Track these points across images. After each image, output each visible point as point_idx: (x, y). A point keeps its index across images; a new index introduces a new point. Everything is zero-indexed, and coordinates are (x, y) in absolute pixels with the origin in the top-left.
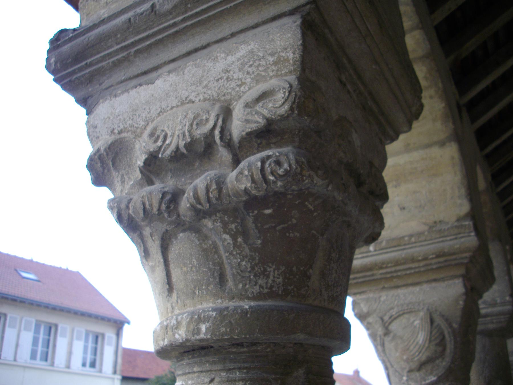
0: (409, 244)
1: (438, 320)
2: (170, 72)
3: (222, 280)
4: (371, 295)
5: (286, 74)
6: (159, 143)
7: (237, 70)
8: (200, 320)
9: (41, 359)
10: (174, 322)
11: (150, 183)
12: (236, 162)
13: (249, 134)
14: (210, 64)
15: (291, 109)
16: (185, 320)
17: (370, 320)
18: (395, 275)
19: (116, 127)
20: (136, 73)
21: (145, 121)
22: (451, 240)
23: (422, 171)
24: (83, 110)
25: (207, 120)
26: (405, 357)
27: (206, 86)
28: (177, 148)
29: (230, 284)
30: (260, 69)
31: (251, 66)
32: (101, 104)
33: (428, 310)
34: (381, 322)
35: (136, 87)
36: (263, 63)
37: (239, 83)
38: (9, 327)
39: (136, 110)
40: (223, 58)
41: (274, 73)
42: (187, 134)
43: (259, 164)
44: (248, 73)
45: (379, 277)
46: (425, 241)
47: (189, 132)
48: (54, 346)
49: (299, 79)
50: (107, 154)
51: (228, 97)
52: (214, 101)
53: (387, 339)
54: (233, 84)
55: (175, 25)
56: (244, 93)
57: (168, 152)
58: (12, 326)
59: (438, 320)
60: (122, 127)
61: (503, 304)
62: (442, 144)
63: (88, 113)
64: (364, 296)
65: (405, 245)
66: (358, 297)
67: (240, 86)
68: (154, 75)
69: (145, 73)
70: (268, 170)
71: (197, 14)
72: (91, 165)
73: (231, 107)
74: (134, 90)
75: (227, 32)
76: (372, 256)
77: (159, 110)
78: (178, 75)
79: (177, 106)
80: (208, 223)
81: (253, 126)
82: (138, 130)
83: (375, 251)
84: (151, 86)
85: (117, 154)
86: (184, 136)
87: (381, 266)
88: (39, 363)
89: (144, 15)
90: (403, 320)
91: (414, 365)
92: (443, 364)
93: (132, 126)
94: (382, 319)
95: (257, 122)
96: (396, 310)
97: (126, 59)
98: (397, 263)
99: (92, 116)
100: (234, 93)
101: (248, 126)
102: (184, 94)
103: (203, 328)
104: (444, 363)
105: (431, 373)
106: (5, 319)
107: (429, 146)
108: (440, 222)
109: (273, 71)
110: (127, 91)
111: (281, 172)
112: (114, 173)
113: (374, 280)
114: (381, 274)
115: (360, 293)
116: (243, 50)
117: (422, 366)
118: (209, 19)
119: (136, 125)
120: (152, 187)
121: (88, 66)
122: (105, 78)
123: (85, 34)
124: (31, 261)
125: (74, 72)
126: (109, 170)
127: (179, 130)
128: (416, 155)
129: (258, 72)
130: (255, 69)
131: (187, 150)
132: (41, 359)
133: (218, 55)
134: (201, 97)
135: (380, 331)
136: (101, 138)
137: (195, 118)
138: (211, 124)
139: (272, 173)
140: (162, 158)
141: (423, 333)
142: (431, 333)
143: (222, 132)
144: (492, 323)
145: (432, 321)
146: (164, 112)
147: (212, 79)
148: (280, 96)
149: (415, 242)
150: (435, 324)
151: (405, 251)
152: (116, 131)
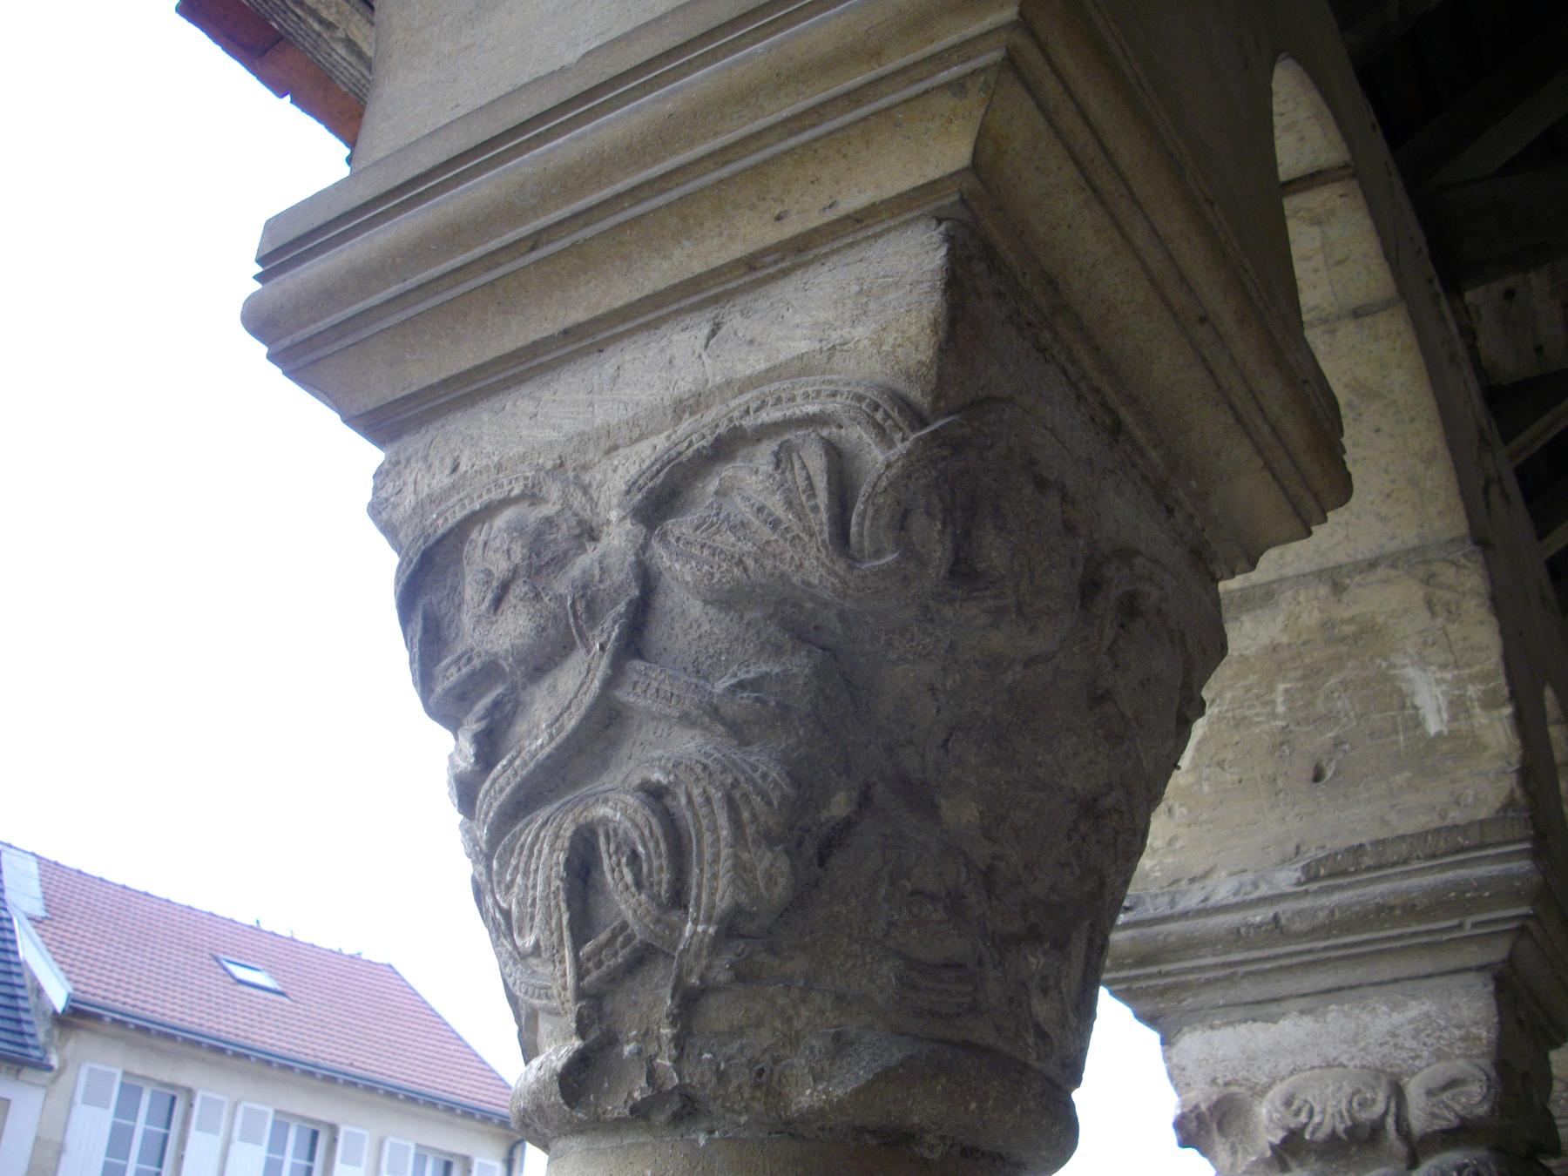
2: (1302, 1012)
5: (1477, 1056)
6: (1303, 1118)
7: (1409, 1037)
13: (1435, 1133)
15: (1492, 1110)
19: (1220, 1075)
20: (1244, 1001)
21: (1269, 1077)
24: (1152, 1037)
25: (1374, 1101)
27: (1363, 1049)
28: (1334, 1132)
30: (1442, 1042)
31: (1428, 1036)
32: (1187, 1035)
35: (1246, 1022)
36: (1445, 1034)
37: (1412, 1054)
38: (344, 1161)
39: (1253, 1059)
40: (1384, 1013)
41: (1461, 1051)
42: (1346, 1114)
44: (1425, 1044)
47: (1348, 1111)
48: (180, 1159)
50: (1211, 1114)
51: (1396, 1070)
52: (1378, 1072)
54: (1404, 1055)
55: (1311, 951)
56: (1421, 1069)
58: (209, 1127)
60: (1229, 1077)
61: (1521, 840)
63: (1166, 1042)
67: (1414, 1058)
68: (1274, 1009)
71: (1345, 946)
72: (1180, 1124)
73: (1402, 1083)
74: (1244, 1026)
75: (1387, 975)
77: (1292, 1067)
78: (1316, 1021)
79: (1320, 1067)
82: (1258, 1087)
84: (1273, 1027)
85: (1224, 1114)
86: (1342, 1116)
89: (1263, 929)
93: (1247, 1079)
95: (1449, 1120)
97: (1230, 978)
99: (1174, 1050)
100: (1404, 1066)
101: (1435, 1121)
102: (1332, 1053)
106: (333, 1141)
109: (1460, 1048)
112: (1216, 1137)
116: (1415, 1010)
118: (1364, 955)
119: (1254, 1080)
121: (1160, 974)
122: (1188, 994)
123: (1153, 925)
124: (256, 929)
125: (1137, 978)
126: (1208, 1132)
127: (1334, 1106)
129: (1439, 1045)
130: (1435, 1041)
131: (1348, 1136)
133: (1377, 1005)
134: (1358, 1063)
136: (1193, 1086)
137: (1354, 1094)
140: (1311, 1142)
141: (669, 604)
146: (1301, 1071)
147: (1372, 1041)
152: (1220, 1081)
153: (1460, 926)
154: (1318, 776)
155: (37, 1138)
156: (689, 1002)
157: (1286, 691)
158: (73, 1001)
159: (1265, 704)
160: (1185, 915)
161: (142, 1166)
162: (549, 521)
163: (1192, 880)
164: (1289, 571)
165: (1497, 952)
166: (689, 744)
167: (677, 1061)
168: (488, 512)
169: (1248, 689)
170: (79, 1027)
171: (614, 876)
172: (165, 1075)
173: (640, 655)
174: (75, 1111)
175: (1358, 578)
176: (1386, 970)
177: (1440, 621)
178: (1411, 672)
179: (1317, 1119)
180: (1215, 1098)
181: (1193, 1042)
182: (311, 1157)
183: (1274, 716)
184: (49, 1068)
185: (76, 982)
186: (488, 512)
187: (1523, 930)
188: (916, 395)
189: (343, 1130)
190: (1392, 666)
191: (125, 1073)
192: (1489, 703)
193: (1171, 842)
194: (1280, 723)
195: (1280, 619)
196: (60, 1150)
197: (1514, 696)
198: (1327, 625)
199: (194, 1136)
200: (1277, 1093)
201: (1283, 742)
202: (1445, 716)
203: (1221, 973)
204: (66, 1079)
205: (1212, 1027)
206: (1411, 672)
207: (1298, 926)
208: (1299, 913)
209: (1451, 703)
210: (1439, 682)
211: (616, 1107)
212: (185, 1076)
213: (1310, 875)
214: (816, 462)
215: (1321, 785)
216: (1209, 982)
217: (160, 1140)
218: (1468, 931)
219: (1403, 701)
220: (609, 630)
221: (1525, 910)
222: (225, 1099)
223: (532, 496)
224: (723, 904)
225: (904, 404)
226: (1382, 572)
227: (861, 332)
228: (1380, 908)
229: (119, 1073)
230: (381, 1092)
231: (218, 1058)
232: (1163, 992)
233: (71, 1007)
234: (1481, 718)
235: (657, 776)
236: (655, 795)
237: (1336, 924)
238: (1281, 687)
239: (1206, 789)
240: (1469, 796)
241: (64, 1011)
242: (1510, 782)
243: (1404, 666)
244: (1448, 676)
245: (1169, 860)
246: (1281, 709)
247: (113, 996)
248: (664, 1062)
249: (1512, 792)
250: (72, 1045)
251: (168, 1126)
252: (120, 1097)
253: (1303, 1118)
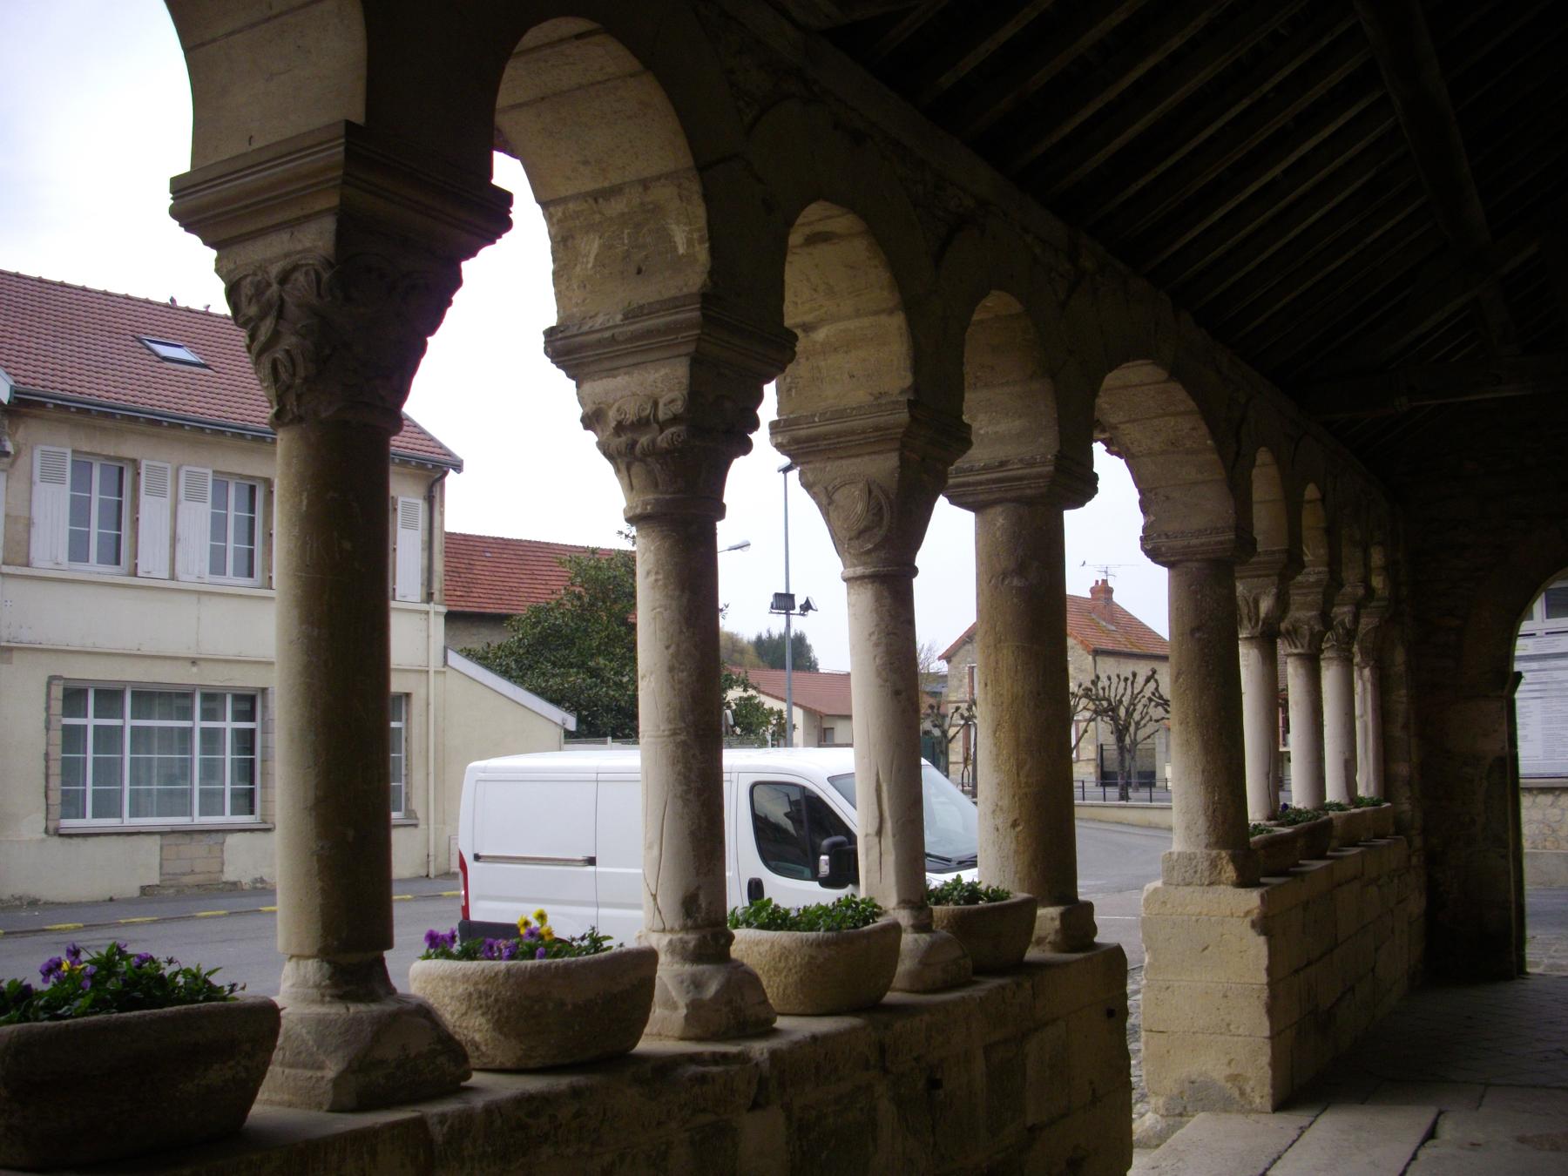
0: (850, 417)
1: (876, 492)
2: (625, 374)
3: (656, 485)
4: (818, 465)
6: (623, 416)
8: (647, 504)
9: (102, 560)
10: (635, 505)
11: (620, 436)
12: (662, 431)
14: (646, 375)
16: (640, 504)
17: (815, 489)
18: (838, 446)
22: (888, 415)
23: (872, 339)
24: (573, 383)
26: (846, 526)
29: (661, 487)
33: (867, 481)
34: (824, 491)
43: (671, 436)
45: (823, 447)
46: (865, 414)
49: (688, 394)
52: (649, 397)
53: (831, 508)
55: (627, 349)
57: (628, 423)
59: (876, 492)
61: (1043, 464)
62: (891, 312)
63: (578, 386)
64: (811, 466)
65: (847, 417)
66: (805, 466)
68: (615, 372)
69: (611, 370)
70: (674, 439)
72: (583, 420)
76: (816, 427)
80: (649, 459)
81: (667, 417)
83: (820, 422)
87: (825, 436)
88: (94, 568)
90: (844, 491)
91: (853, 534)
92: (880, 533)
94: (826, 488)
96: (839, 480)
98: (839, 435)
103: (649, 507)
104: (881, 532)
105: (869, 541)
107: (876, 313)
108: (885, 393)
110: (601, 379)
111: (680, 440)
113: (819, 451)
114: (825, 445)
115: (807, 463)
116: (663, 372)
117: (860, 534)
120: (621, 439)
128: (866, 321)
132: (101, 560)
135: (825, 501)
138: (648, 411)
139: (677, 441)
142: (869, 503)
143: (654, 416)
144: (1031, 488)
145: (870, 492)
148: (679, 403)
149: (855, 415)
150: (874, 494)
151: (846, 424)
153: (677, 338)
154: (639, 272)
155: (7, 516)
156: (299, 397)
157: (629, 233)
158: (16, 392)
159: (620, 239)
160: (582, 334)
161: (100, 531)
162: (259, 281)
163: (591, 318)
164: (627, 180)
165: (691, 348)
166: (294, 339)
167: (298, 409)
168: (246, 276)
169: (614, 232)
170: (26, 415)
171: (281, 369)
172: (110, 450)
173: (282, 318)
174: (35, 489)
175: (653, 183)
176: (657, 355)
177: (684, 204)
178: (674, 227)
179: (628, 416)
180: (594, 409)
181: (587, 387)
182: (252, 509)
183: (624, 244)
184: (7, 454)
185: (15, 375)
186: (246, 276)
187: (699, 339)
188: (332, 261)
189: (144, 464)
190: (667, 223)
191: (74, 452)
192: (701, 242)
193: (584, 301)
194: (626, 248)
195: (625, 201)
196: (29, 523)
197: (711, 238)
198: (642, 204)
199: (145, 500)
200: (615, 407)
201: (627, 256)
202: (685, 246)
203: (597, 358)
204: (22, 462)
205: (594, 381)
206: (674, 227)
207: (621, 338)
208: (621, 333)
209: (687, 241)
210: (684, 231)
211: (286, 420)
212: (128, 449)
213: (626, 317)
214: (312, 274)
215: (640, 276)
216: (592, 362)
217: (115, 508)
218: (679, 340)
219: (669, 239)
220: (274, 313)
221: (698, 332)
222: (168, 465)
223: (255, 274)
224: (303, 375)
225: (329, 262)
226: (662, 181)
227: (320, 244)
228: (648, 331)
229: (69, 452)
230: (414, 464)
231: (155, 430)
232: (577, 366)
233: (15, 398)
234: (697, 248)
235: (287, 348)
236: (287, 352)
237: (635, 337)
238: (626, 231)
239: (598, 276)
240: (691, 283)
241: (9, 402)
242: (705, 276)
243: (671, 224)
244: (687, 229)
245: (583, 309)
246: (626, 241)
247: (32, 381)
248: (295, 410)
249: (705, 281)
250: (21, 434)
251: (120, 494)
252: (73, 469)
253: (623, 416)
